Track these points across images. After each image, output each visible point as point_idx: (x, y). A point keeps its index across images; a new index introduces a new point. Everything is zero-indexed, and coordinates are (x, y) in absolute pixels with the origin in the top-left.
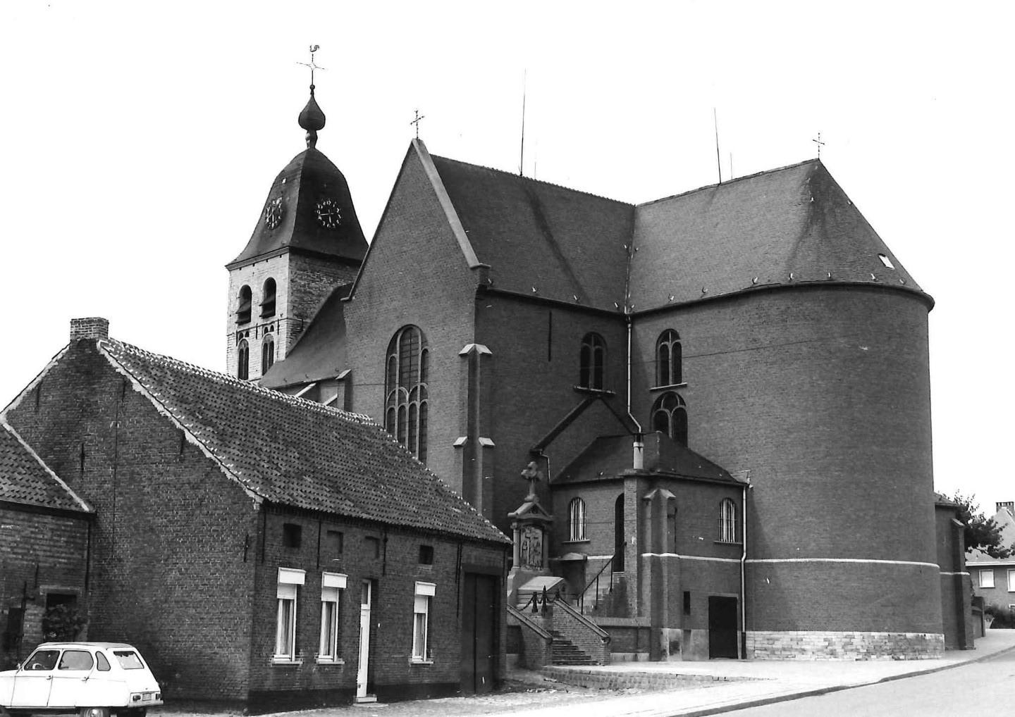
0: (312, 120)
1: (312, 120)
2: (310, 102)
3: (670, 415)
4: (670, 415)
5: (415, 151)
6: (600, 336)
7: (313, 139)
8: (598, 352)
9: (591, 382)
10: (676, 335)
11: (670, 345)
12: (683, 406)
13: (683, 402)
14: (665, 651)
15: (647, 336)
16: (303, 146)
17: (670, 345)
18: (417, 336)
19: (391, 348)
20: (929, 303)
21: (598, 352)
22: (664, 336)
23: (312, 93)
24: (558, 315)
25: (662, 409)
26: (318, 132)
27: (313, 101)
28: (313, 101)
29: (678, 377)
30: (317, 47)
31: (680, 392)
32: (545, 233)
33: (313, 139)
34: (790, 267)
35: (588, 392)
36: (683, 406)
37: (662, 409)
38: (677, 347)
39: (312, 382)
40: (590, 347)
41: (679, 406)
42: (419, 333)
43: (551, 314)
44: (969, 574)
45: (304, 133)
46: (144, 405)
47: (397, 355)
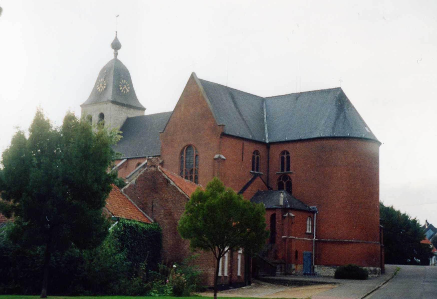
0: (116, 46)
1: (116, 46)
2: (115, 39)
3: (285, 183)
4: (285, 183)
5: (193, 77)
6: (259, 151)
7: (116, 54)
8: (258, 158)
9: (255, 169)
10: (288, 153)
11: (285, 156)
12: (290, 180)
13: (290, 178)
14: (424, 283)
15: (276, 153)
16: (113, 57)
17: (285, 156)
18: (193, 149)
19: (182, 152)
20: (380, 144)
21: (258, 158)
22: (283, 153)
23: (116, 35)
24: (246, 143)
25: (281, 180)
26: (118, 51)
27: (116, 39)
28: (116, 39)
29: (288, 169)
30: (118, 15)
31: (289, 175)
32: (237, 110)
33: (116, 54)
34: (333, 129)
35: (254, 173)
36: (290, 180)
37: (281, 180)
38: (288, 158)
39: (125, 159)
40: (255, 156)
41: (289, 180)
42: (194, 147)
43: (243, 143)
44: (434, 257)
45: (113, 50)
46: (175, 190)
47: (184, 156)
